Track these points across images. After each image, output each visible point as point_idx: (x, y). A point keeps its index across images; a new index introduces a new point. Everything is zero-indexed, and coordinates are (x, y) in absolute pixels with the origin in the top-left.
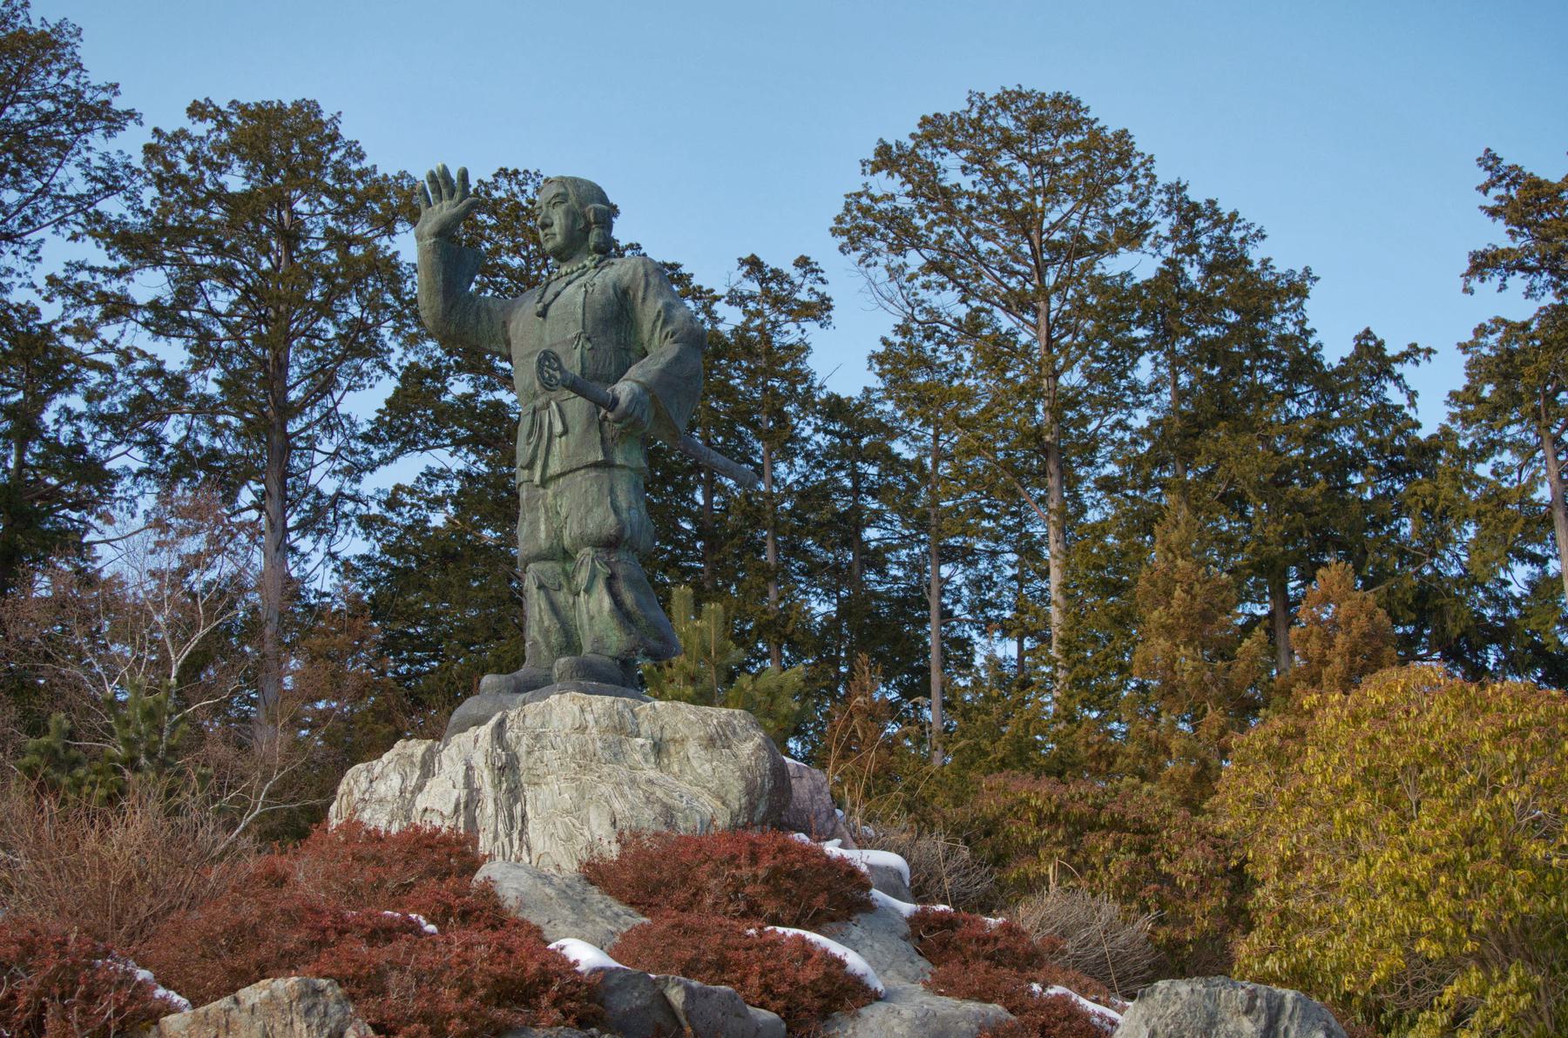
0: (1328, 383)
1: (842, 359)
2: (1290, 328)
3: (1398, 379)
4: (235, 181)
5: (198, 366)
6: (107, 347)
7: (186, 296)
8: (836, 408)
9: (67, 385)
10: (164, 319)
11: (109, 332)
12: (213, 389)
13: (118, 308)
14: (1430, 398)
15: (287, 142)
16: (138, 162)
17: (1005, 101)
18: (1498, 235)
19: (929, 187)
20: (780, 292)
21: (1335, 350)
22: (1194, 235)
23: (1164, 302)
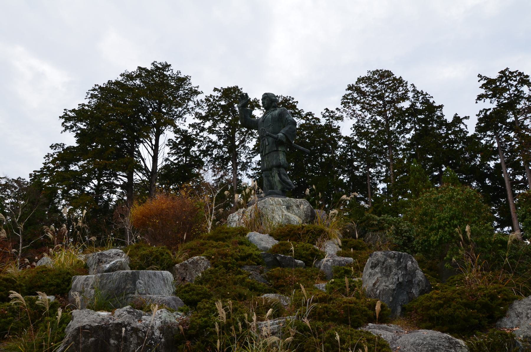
0: (449, 126)
1: (346, 128)
2: (439, 114)
3: (463, 123)
4: (223, 103)
5: (219, 140)
6: (202, 137)
7: (214, 125)
8: (347, 138)
9: (194, 145)
10: (211, 130)
11: (201, 134)
12: (222, 143)
13: (203, 130)
14: (470, 127)
15: (232, 94)
16: (203, 100)
17: (374, 73)
18: (483, 91)
19: (358, 90)
20: (330, 114)
21: (450, 120)
22: (418, 97)
23: (413, 111)
